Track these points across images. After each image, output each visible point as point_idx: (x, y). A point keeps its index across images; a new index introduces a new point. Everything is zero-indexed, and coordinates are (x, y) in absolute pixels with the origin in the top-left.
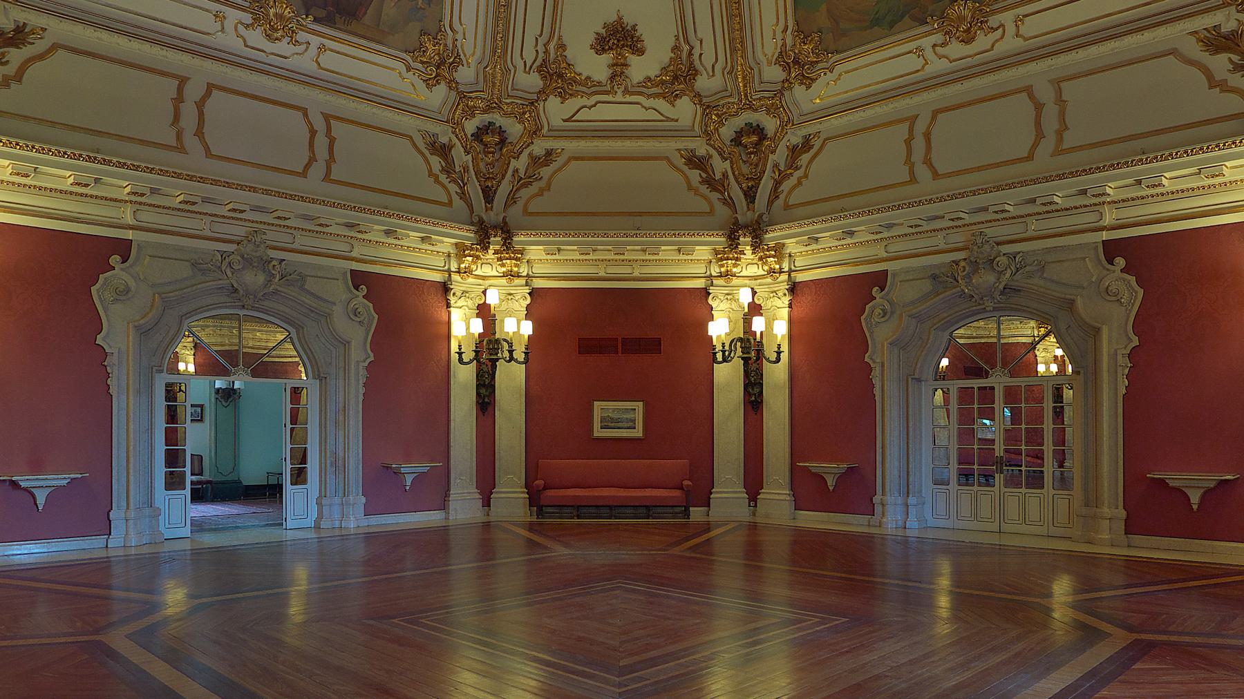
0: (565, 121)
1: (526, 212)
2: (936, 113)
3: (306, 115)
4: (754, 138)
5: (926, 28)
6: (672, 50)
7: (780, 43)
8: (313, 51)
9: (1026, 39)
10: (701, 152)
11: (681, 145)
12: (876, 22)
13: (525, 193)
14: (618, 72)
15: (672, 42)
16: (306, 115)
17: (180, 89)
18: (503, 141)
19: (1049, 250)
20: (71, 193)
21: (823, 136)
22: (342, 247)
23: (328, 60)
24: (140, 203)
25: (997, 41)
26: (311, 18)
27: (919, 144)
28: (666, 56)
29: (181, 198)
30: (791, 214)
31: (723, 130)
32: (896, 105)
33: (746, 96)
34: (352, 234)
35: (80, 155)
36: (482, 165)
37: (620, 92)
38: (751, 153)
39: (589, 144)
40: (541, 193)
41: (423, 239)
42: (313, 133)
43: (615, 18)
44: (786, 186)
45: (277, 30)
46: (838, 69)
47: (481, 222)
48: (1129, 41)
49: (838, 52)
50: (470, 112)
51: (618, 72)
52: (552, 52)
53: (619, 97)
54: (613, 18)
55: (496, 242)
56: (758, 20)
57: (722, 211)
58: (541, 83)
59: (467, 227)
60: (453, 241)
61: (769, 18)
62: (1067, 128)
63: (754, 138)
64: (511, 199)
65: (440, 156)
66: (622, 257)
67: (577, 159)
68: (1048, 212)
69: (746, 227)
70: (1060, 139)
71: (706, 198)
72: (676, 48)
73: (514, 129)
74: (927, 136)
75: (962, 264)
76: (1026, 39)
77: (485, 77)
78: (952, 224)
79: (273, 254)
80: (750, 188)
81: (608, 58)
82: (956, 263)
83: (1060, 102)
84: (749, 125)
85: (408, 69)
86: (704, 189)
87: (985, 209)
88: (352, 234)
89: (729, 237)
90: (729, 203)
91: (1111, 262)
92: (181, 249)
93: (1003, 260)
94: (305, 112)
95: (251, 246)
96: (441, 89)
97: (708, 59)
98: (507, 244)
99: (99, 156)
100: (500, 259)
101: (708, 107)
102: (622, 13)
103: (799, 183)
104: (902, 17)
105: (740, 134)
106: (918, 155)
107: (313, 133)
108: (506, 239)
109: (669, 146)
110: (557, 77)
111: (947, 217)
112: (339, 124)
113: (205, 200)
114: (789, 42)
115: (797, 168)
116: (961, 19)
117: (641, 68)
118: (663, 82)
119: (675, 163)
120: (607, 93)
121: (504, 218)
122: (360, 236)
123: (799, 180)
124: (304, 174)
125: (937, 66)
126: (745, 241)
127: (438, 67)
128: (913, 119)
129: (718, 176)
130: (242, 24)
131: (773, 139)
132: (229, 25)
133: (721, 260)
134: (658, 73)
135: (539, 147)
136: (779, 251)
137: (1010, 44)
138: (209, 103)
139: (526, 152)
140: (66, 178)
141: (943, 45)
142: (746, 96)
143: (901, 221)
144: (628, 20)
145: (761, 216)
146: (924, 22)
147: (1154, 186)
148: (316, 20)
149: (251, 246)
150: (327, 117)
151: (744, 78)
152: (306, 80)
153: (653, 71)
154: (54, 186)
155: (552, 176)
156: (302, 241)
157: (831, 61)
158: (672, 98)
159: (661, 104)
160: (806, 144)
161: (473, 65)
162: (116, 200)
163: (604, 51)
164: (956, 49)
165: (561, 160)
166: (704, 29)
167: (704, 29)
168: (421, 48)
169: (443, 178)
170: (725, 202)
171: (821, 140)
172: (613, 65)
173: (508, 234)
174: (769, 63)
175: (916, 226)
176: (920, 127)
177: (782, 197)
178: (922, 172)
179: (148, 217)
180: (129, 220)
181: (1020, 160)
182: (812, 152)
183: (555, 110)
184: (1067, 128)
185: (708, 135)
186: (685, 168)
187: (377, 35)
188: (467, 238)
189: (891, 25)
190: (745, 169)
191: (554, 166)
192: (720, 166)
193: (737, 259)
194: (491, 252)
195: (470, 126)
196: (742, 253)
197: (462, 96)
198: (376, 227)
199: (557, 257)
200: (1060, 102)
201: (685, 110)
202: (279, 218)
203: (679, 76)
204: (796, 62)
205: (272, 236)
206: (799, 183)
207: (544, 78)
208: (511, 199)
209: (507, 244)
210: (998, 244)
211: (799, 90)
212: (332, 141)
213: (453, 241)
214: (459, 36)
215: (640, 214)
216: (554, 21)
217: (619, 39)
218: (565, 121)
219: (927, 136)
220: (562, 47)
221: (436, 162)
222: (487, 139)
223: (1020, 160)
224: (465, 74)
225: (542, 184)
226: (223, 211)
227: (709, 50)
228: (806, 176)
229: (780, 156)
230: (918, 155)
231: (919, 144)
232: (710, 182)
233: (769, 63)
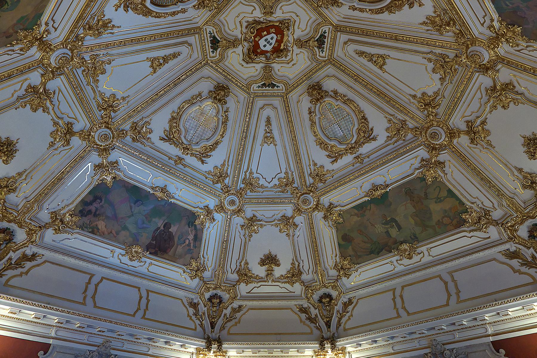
0: (247, 293)
1: (229, 333)
2: (403, 288)
3: (139, 290)
4: (328, 300)
5: (392, 254)
6: (291, 264)
7: (335, 261)
8: (147, 264)
9: (433, 257)
10: (305, 306)
11: (296, 303)
12: (372, 252)
13: (229, 324)
14: (270, 273)
15: (291, 261)
16: (139, 290)
17: (90, 279)
18: (221, 302)
19: (467, 347)
20: (31, 322)
21: (357, 298)
22: (144, 349)
23: (153, 269)
24: (60, 327)
25: (422, 258)
26: (148, 252)
27: (398, 300)
28: (289, 266)
29: (78, 325)
30: (347, 333)
31: (314, 296)
32: (386, 284)
33: (323, 282)
34: (150, 343)
35: (41, 305)
36: (211, 312)
37: (270, 281)
38: (327, 306)
39: (257, 303)
40: (236, 324)
41: (181, 346)
42: (141, 298)
43: (268, 252)
44: (344, 320)
45: (134, 257)
46: (360, 270)
47: (209, 337)
48: (474, 256)
49: (359, 264)
50: (208, 289)
51: (270, 273)
52: (243, 265)
53: (270, 283)
54: (267, 252)
55: (215, 346)
56: (324, 249)
57: (316, 332)
58: (238, 278)
59: (202, 340)
60: (195, 347)
61: (329, 252)
62: (460, 292)
63: (328, 300)
64: (223, 328)
65: (194, 308)
66: (272, 355)
67: (252, 309)
68: (462, 329)
69: (328, 339)
70: (458, 296)
71: (309, 326)
72: (293, 264)
73: (226, 296)
74: (401, 297)
75: (429, 355)
76: (433, 257)
77: (215, 275)
78: (420, 336)
79: (113, 352)
80: (328, 321)
81: (265, 268)
82: (426, 354)
83: (454, 280)
84: (325, 294)
85: (184, 272)
86: (308, 322)
87: (434, 328)
88: (150, 343)
89: (320, 344)
90: (319, 329)
91: (498, 352)
92: (71, 349)
93: (448, 352)
94: (139, 289)
95: (104, 348)
96: (197, 280)
97: (306, 268)
98: (220, 348)
99: (49, 306)
100: (216, 356)
101: (307, 287)
102: (271, 251)
103: (349, 319)
104: (382, 250)
105: (321, 298)
106: (399, 305)
107: (141, 298)
108: (219, 346)
109: (292, 303)
110: (245, 275)
111: (418, 332)
112: (153, 294)
113: (89, 326)
114: (338, 260)
115: (348, 312)
116: (406, 250)
117: (278, 271)
118: (288, 277)
119: (295, 311)
120: (265, 281)
121: (219, 336)
122: (153, 344)
123: (349, 317)
124: (134, 315)
125: (399, 268)
126: (328, 346)
127: (196, 271)
128: (394, 290)
129: (313, 316)
130: (121, 254)
131: (336, 300)
132: (116, 255)
133: (317, 355)
134: (286, 273)
135: (235, 305)
136: (343, 350)
137: (427, 259)
138: (100, 285)
139: (230, 306)
140: (30, 315)
141: (401, 260)
142: (323, 282)
143: (397, 335)
144: (273, 253)
145: (334, 334)
146: (391, 252)
147: (506, 315)
148: (150, 253)
149: (104, 348)
150: (148, 291)
151: (321, 275)
152: (142, 276)
153: (284, 273)
154: (25, 318)
155: (241, 317)
156: (127, 346)
157: (356, 267)
158: (292, 283)
159: (287, 286)
160: (350, 302)
161: (210, 271)
162: (50, 325)
163: (264, 265)
164: (406, 261)
165: (245, 310)
166: (304, 256)
167: (304, 256)
168: (190, 264)
169: (194, 317)
170: (317, 328)
171: (356, 300)
172: (268, 270)
173: (220, 342)
174: (331, 269)
175: (405, 337)
176: (398, 293)
177: (342, 325)
178: (402, 312)
179: (62, 334)
180: (53, 334)
181: (444, 306)
182: (353, 305)
183: (243, 289)
184: (460, 292)
185: (308, 299)
186: (299, 313)
187: (174, 259)
188: (202, 345)
189: (378, 253)
190: (325, 313)
191: (242, 312)
192: (314, 312)
193: (325, 355)
194: (212, 352)
195: (207, 295)
196: (327, 352)
197: (205, 283)
198: (161, 340)
199: (242, 355)
200: (454, 280)
201: (297, 288)
202: (119, 335)
203: (295, 275)
204: (342, 268)
205: (115, 344)
206: (349, 319)
207: (239, 276)
208: (223, 328)
209: (220, 348)
210: (444, 344)
211: (344, 279)
212: (148, 301)
213: (195, 347)
214: (206, 260)
215: (280, 334)
216: (244, 253)
217: (270, 260)
218: (247, 293)
219: (401, 297)
220: (247, 263)
221: (191, 311)
222: (214, 301)
223: (444, 306)
224: (207, 274)
225: (237, 320)
226: (95, 331)
227: (306, 264)
228: (352, 315)
229: (339, 307)
230: (399, 305)
231: (398, 300)
232: (309, 319)
233: (331, 269)
